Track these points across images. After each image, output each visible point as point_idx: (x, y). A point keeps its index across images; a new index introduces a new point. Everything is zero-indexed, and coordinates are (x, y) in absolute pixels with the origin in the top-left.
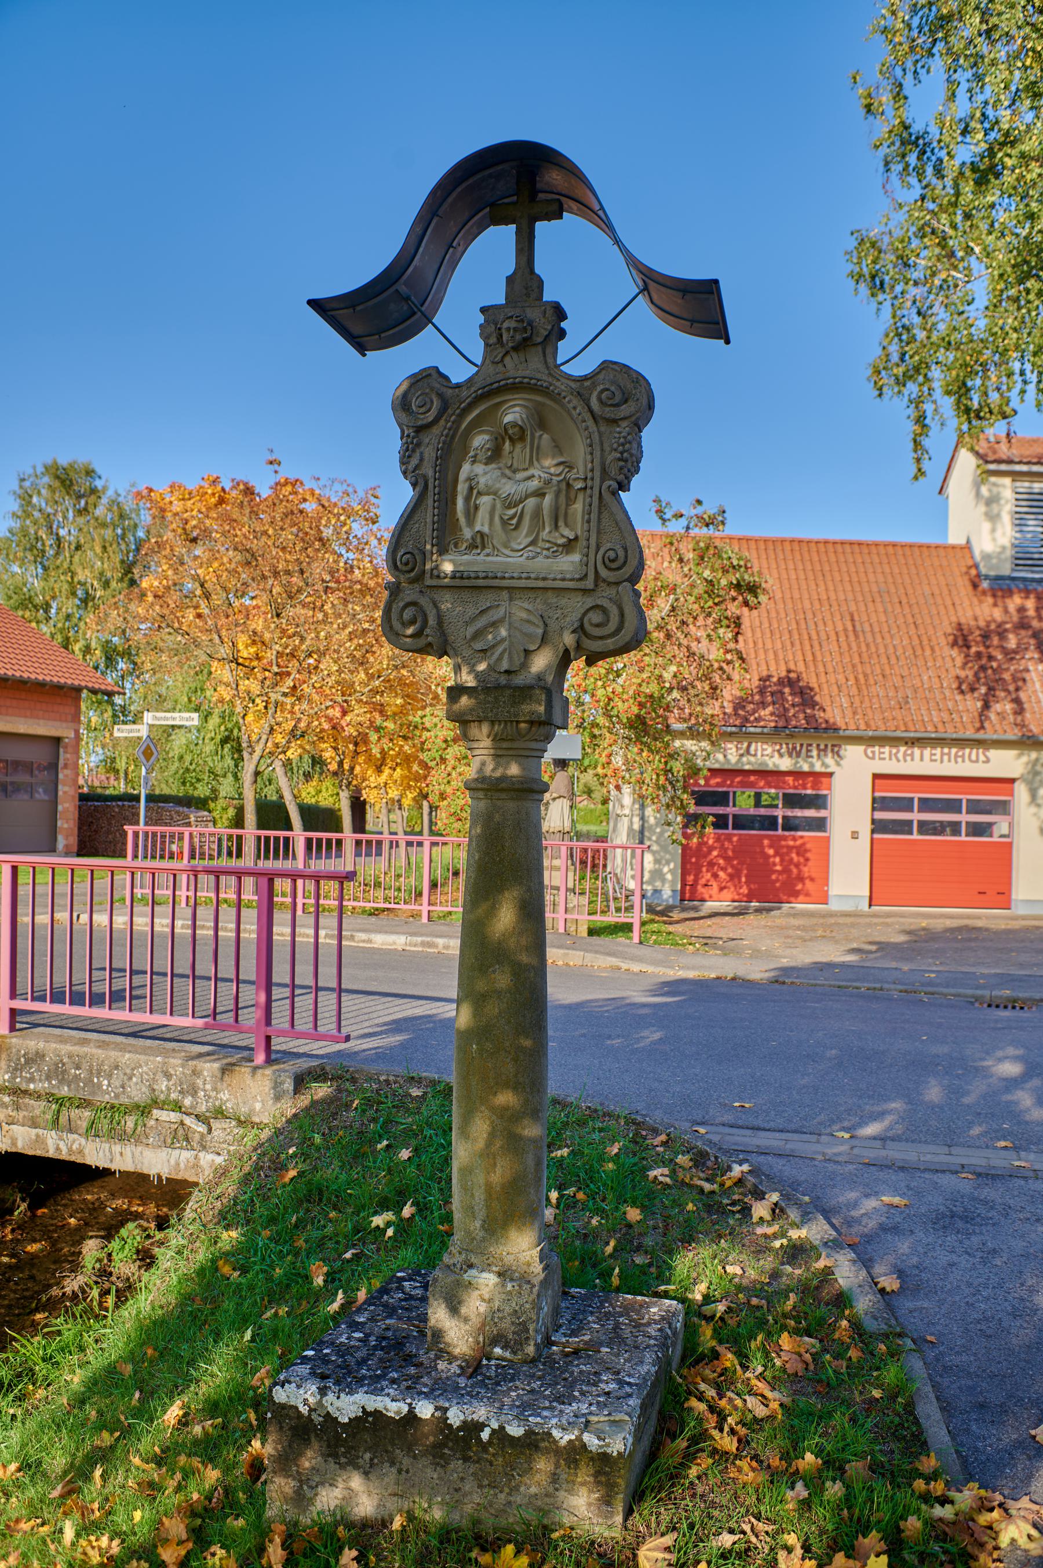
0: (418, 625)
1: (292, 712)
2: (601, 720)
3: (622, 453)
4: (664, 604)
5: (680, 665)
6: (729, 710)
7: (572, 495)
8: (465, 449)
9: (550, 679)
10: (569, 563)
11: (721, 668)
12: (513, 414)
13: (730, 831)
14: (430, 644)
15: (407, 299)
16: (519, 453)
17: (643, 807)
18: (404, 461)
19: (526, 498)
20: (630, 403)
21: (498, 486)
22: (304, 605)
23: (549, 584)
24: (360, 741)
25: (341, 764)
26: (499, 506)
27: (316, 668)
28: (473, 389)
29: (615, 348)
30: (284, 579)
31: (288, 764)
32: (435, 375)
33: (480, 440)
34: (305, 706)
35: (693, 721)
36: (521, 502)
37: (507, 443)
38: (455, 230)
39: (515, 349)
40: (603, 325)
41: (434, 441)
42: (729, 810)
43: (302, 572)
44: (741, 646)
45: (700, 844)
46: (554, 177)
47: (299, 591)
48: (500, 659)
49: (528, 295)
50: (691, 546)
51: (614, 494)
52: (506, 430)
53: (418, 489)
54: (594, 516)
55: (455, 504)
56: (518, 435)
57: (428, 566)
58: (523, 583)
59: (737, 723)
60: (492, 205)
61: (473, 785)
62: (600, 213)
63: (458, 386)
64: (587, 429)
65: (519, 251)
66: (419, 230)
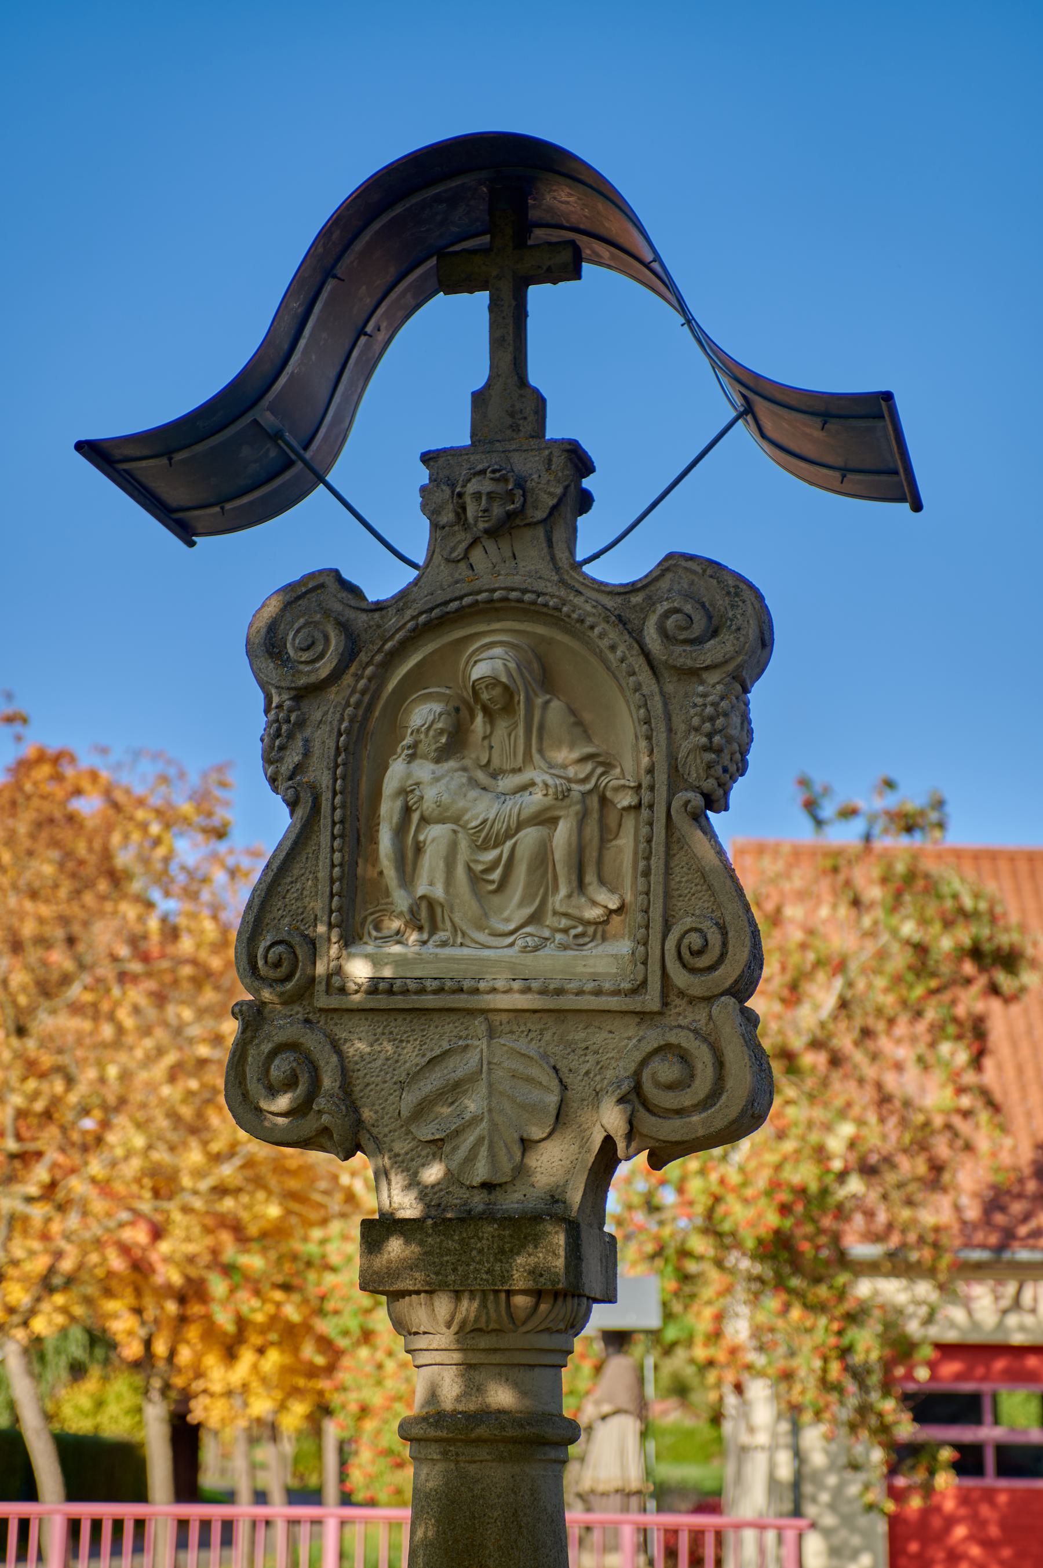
0: (301, 1089)
1: (45, 1237)
2: (699, 1244)
3: (710, 736)
4: (823, 995)
5: (861, 1122)
6: (973, 1213)
7: (612, 820)
8: (394, 727)
9: (575, 1196)
10: (609, 959)
11: (948, 1127)
12: (489, 662)
13: (990, 1481)
14: (326, 1131)
15: (276, 436)
16: (503, 739)
17: (796, 1429)
18: (272, 755)
19: (518, 829)
20: (725, 635)
21: (461, 804)
22: (76, 1009)
23: (567, 1002)
24: (193, 1292)
25: (148, 1343)
26: (463, 844)
27: (99, 1140)
28: (409, 613)
29: (692, 528)
30: (33, 954)
31: (36, 1351)
32: (333, 586)
33: (424, 714)
34: (73, 1221)
35: (894, 1241)
36: (508, 836)
37: (479, 719)
38: (369, 302)
39: (492, 533)
40: (664, 481)
41: (333, 717)
42: (987, 1433)
43: (71, 941)
44: (990, 1076)
45: (926, 1513)
46: (563, 199)
47: (66, 980)
48: (471, 1158)
49: (515, 428)
50: (876, 872)
51: (698, 819)
52: (475, 693)
53: (300, 812)
54: (657, 863)
55: (374, 841)
56: (500, 702)
57: (321, 969)
59: (993, 1239)
60: (441, 253)
61: (416, 1431)
62: (656, 266)
63: (379, 607)
64: (638, 688)
65: (496, 343)
66: (297, 306)
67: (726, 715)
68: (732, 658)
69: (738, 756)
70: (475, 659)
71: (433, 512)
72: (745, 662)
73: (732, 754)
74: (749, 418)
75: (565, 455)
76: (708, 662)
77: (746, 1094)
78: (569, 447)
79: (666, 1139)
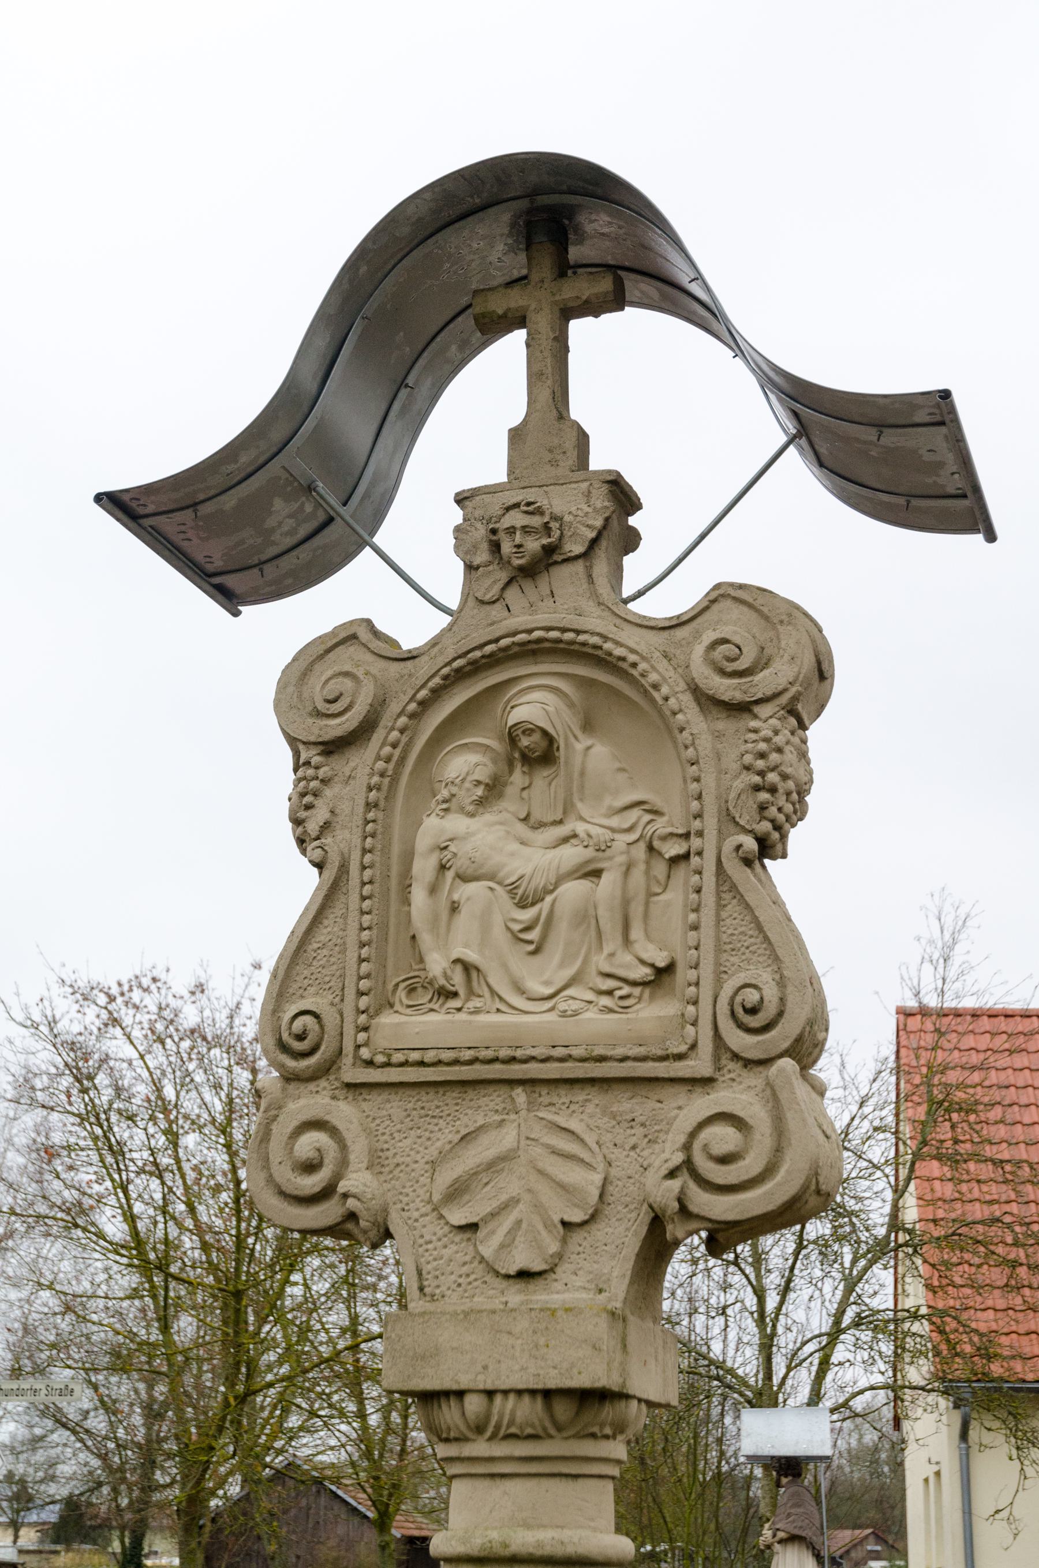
40: (715, 503)
58: (552, 1070)
67: (779, 750)
68: (785, 690)
69: (795, 796)
70: (512, 704)
71: (466, 553)
72: (800, 693)
73: (788, 794)
74: (803, 442)
75: (606, 486)
76: (760, 695)
77: (807, 1167)
78: (609, 478)
79: (719, 1218)
